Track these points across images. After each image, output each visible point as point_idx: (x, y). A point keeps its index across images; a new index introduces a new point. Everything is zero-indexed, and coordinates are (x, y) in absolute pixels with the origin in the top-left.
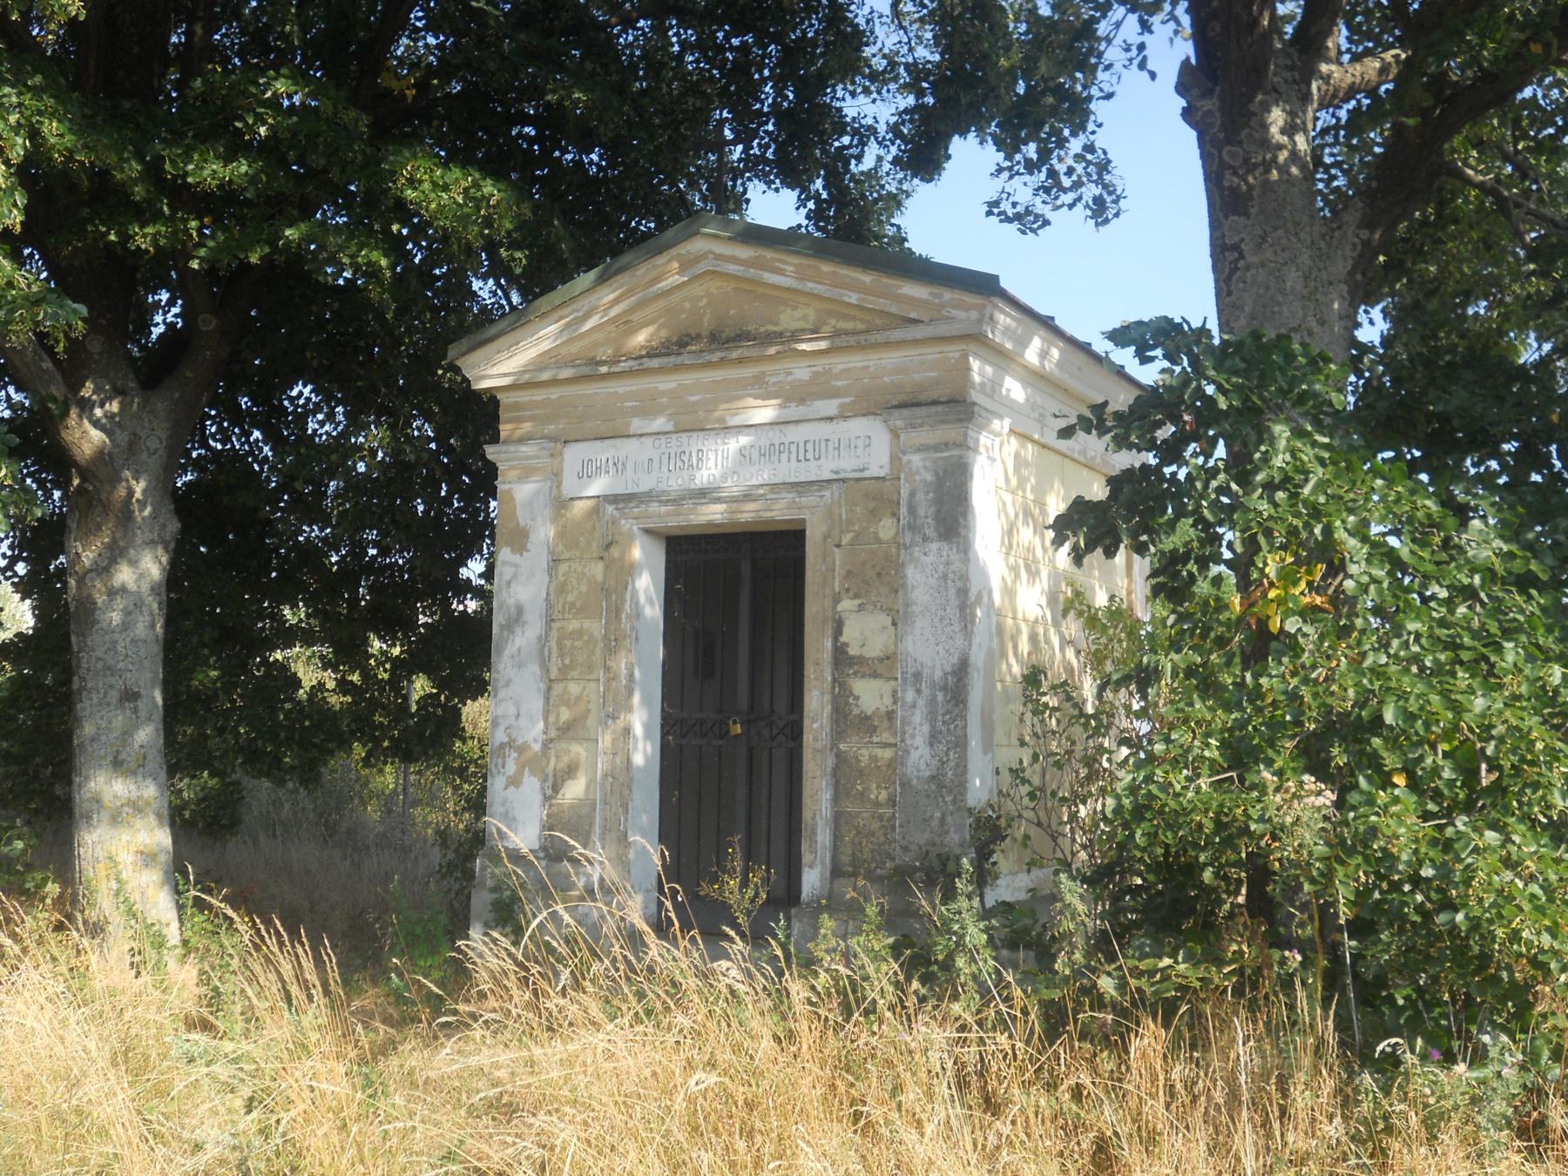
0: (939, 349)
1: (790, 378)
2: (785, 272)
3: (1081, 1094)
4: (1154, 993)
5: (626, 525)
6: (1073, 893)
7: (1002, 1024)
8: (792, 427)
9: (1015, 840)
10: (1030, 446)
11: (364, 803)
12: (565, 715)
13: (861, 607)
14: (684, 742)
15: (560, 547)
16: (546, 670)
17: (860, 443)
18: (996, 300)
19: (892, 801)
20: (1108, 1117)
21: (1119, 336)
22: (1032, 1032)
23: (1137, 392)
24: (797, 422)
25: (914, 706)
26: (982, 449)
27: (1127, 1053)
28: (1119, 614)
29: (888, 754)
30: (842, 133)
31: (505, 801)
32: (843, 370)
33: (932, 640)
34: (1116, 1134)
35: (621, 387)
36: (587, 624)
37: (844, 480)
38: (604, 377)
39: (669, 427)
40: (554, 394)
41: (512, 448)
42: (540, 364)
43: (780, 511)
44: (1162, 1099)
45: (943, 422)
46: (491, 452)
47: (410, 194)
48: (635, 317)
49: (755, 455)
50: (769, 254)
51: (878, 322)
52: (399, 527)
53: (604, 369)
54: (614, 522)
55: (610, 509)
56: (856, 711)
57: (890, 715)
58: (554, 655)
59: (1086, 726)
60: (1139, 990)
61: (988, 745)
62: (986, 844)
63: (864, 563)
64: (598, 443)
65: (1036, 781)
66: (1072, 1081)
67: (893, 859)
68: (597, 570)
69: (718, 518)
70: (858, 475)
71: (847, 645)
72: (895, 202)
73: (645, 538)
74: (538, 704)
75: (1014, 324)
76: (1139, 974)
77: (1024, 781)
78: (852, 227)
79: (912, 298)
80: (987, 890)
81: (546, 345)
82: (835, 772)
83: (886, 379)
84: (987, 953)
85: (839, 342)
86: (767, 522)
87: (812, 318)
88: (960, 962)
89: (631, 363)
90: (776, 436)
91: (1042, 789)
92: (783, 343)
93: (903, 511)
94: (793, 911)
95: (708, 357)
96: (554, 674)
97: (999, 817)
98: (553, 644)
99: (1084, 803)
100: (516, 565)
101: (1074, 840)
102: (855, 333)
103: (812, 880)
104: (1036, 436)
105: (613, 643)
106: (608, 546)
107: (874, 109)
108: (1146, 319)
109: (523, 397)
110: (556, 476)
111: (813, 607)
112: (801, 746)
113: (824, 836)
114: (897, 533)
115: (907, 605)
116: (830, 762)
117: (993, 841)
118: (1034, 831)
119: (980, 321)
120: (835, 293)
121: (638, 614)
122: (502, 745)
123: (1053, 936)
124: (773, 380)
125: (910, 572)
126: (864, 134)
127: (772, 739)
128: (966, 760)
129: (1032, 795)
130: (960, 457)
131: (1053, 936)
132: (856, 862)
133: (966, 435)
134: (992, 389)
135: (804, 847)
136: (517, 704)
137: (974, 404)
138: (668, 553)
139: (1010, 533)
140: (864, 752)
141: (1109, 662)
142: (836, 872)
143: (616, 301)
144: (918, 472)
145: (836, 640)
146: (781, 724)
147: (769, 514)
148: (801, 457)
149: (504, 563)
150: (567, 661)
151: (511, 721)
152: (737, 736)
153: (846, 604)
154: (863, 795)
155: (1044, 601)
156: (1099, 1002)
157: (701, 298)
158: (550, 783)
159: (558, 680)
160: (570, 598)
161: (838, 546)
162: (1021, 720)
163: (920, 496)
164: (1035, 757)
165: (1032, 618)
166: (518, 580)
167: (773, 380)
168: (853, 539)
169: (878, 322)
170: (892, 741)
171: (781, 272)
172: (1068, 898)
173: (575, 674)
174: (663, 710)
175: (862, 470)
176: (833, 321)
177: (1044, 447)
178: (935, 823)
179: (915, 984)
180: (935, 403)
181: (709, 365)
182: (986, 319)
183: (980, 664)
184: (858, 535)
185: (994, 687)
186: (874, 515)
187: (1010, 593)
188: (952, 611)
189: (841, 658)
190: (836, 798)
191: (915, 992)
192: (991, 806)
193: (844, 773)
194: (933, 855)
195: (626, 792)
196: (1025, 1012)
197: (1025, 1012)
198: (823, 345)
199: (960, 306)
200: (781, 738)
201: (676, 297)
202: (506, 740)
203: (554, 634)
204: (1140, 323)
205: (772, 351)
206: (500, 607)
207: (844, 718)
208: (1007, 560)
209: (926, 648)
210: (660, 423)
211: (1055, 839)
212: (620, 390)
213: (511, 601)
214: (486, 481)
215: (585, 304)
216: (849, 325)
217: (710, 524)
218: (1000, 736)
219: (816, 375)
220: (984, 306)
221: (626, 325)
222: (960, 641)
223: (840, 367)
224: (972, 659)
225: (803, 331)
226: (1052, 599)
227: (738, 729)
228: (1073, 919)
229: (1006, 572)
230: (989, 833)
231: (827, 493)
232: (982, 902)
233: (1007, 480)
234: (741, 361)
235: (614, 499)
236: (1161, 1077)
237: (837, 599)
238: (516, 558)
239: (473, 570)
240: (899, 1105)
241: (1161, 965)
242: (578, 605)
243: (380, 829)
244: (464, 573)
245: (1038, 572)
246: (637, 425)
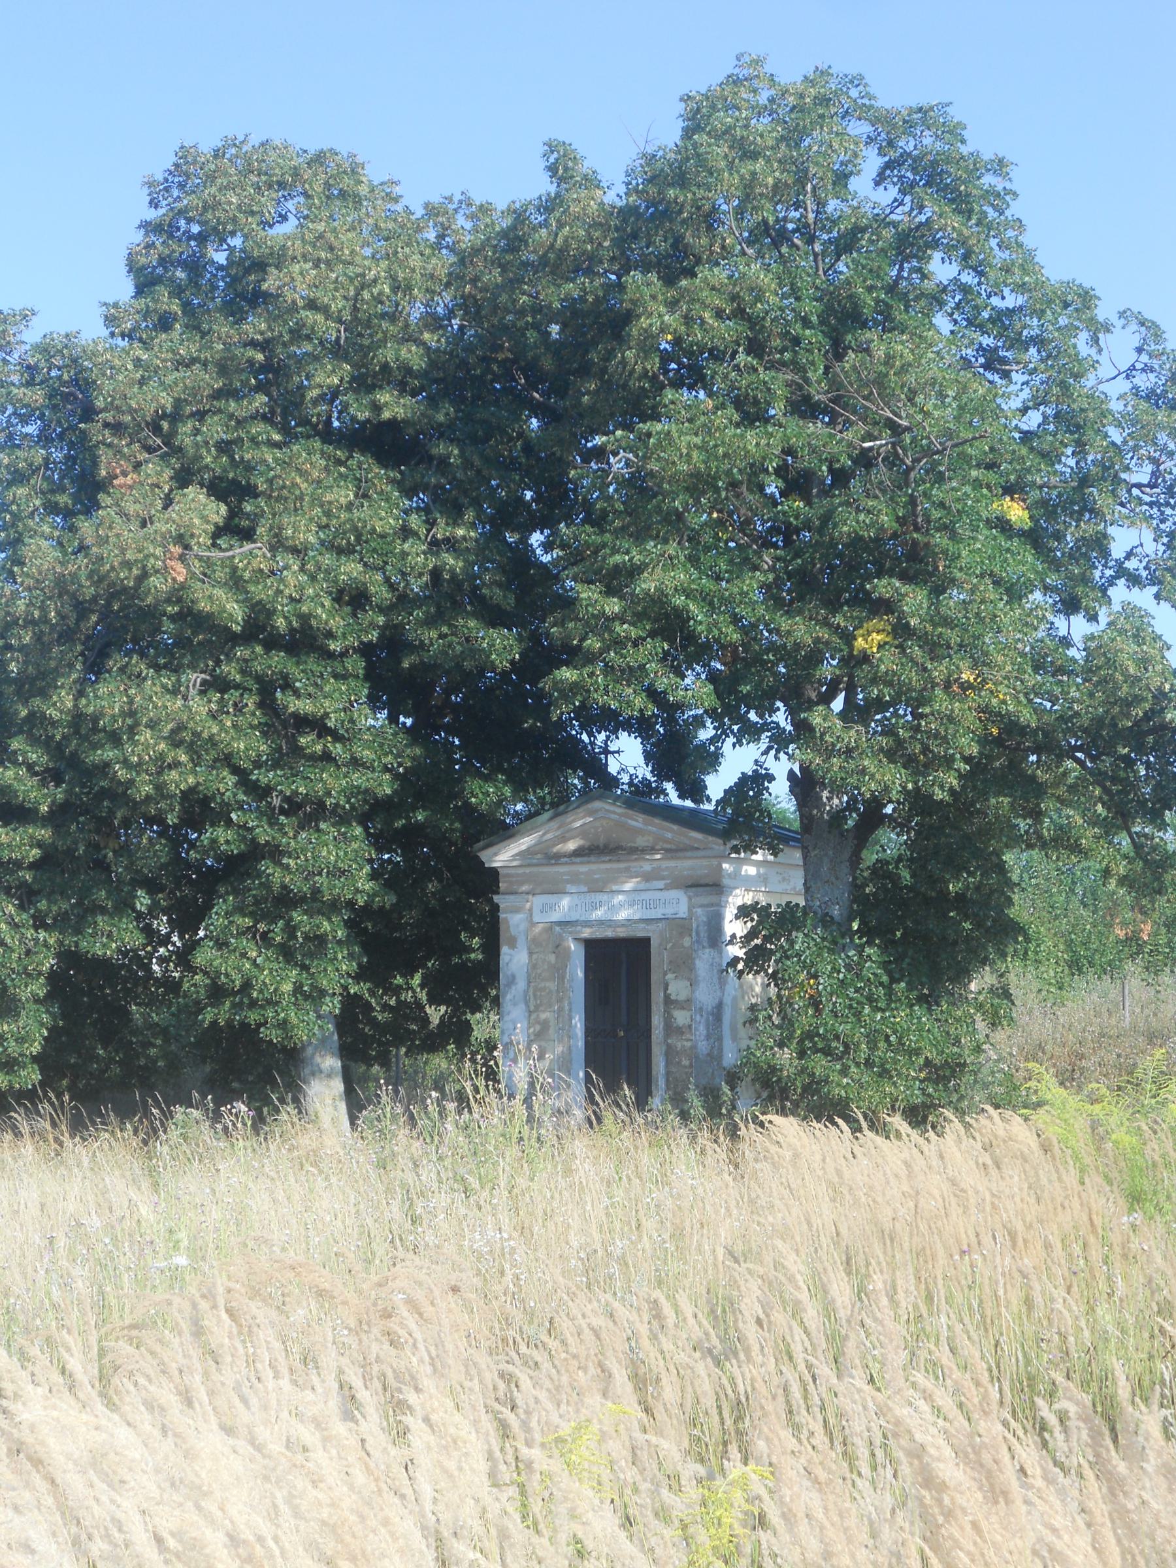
29: (688, 1044)
55: (558, 929)
57: (690, 1026)
61: (735, 1038)
68: (552, 958)
82: (667, 1054)
90: (637, 897)
111: (655, 977)
116: (664, 1048)
125: (697, 962)
140: (680, 1044)
153: (670, 976)
154: (679, 1063)
186: (681, 935)
189: (668, 1001)
190: (667, 1065)
193: (670, 1053)
207: (670, 1028)
209: (705, 996)
222: (719, 993)
237: (665, 974)
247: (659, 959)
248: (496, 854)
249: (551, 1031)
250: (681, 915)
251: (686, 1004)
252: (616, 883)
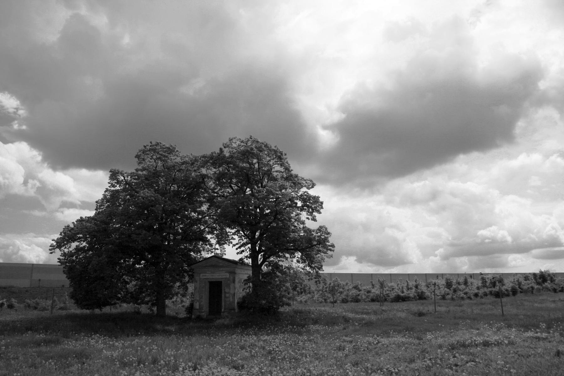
43: (220, 280)
142: (225, 309)
207: (225, 297)
209: (232, 292)
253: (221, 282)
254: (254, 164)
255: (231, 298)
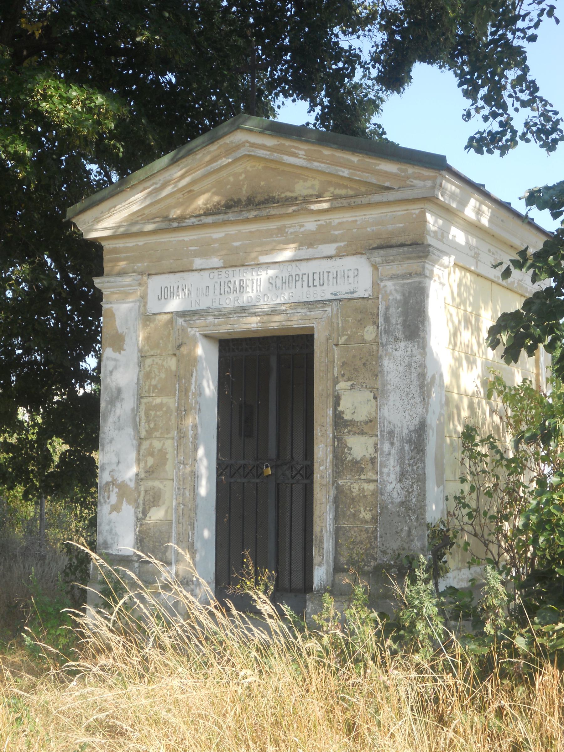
0: (405, 208)
1: (302, 229)
2: (298, 155)
3: (502, 713)
4: (552, 647)
5: (192, 331)
6: (494, 579)
7: (448, 668)
8: (304, 264)
9: (459, 546)
10: (468, 275)
11: (13, 526)
12: (150, 461)
13: (352, 387)
14: (232, 480)
15: (147, 348)
16: (136, 427)
17: (351, 274)
18: (444, 173)
19: (374, 519)
20: (521, 729)
21: (533, 198)
22: (468, 674)
23: (545, 239)
24: (307, 260)
25: (389, 454)
26: (436, 278)
27: (534, 685)
28: (530, 392)
29: (371, 487)
30: (338, 60)
31: (110, 522)
32: (340, 223)
33: (401, 409)
34: (526, 740)
35: (187, 237)
36: (165, 400)
37: (340, 300)
38: (175, 230)
39: (220, 264)
40: (141, 241)
41: (112, 279)
42: (134, 219)
43: (297, 322)
44: (557, 716)
45: (409, 258)
46: (98, 282)
47: (44, 105)
48: (196, 188)
49: (279, 282)
50: (287, 143)
51: (363, 189)
52: (35, 333)
53: (175, 224)
54: (184, 330)
55: (180, 321)
56: (350, 458)
57: (373, 461)
58: (143, 421)
59: (508, 466)
60: (542, 645)
61: (440, 481)
62: (439, 549)
63: (354, 357)
64: (171, 276)
65: (473, 505)
66: (495, 705)
67: (375, 559)
68: (172, 363)
69: (254, 326)
70: (350, 296)
71: (343, 412)
72: (374, 106)
73: (205, 341)
74: (133, 455)
75: (458, 191)
76: (540, 634)
77: (465, 506)
78: (346, 124)
79: (386, 172)
80: (440, 581)
81: (135, 208)
82: (336, 501)
83: (369, 229)
84: (438, 620)
85: (336, 204)
86: (287, 329)
87: (317, 187)
88: (420, 626)
89: (193, 220)
90: (293, 269)
91: (477, 510)
92: (297, 205)
93: (381, 320)
94: (308, 596)
95: (245, 215)
96: (143, 434)
97: (448, 530)
98: (142, 414)
99: (507, 520)
100: (115, 360)
101: (500, 546)
102: (347, 197)
103: (320, 574)
104: (473, 268)
105: (183, 411)
106: (179, 346)
107: (365, 43)
108: (550, 184)
109: (120, 244)
110: (144, 298)
111: (319, 387)
112: (312, 482)
113: (328, 545)
114: (377, 336)
115: (384, 385)
116: (332, 493)
117: (445, 546)
118: (473, 541)
119: (433, 187)
120: (332, 169)
121: (200, 393)
122: (108, 484)
123: (483, 609)
124: (292, 230)
125: (386, 362)
126: (352, 59)
127: (293, 478)
128: (425, 491)
129: (470, 515)
130: (420, 283)
131: (483, 609)
132: (351, 562)
133: (424, 268)
134: (442, 234)
135: (315, 551)
136: (118, 455)
137: (430, 245)
138: (220, 351)
139: (455, 335)
140: (356, 486)
141: (524, 423)
142: (338, 569)
143: (182, 177)
144: (391, 293)
145: (335, 409)
146: (298, 467)
147: (289, 323)
148: (311, 284)
149: (108, 359)
150: (152, 426)
151: (114, 467)
152: (268, 476)
153: (342, 385)
154: (354, 516)
155: (478, 383)
156: (515, 653)
157: (240, 174)
158: (141, 509)
159: (146, 439)
160: (154, 382)
161: (336, 345)
162: (462, 463)
163: (392, 310)
164: (473, 489)
165: (470, 393)
166: (117, 370)
167: (292, 230)
168: (346, 340)
169: (363, 189)
170: (374, 477)
171: (295, 155)
172: (492, 582)
173: (157, 434)
174: (218, 459)
175: (352, 293)
176: (332, 189)
177: (478, 275)
178: (404, 534)
179: (389, 642)
180: (402, 245)
181: (247, 221)
182: (437, 186)
183: (434, 426)
184: (350, 337)
185: (444, 441)
186: (361, 323)
187: (455, 375)
188: (415, 389)
189: (339, 421)
190: (336, 518)
191: (390, 648)
192: (442, 522)
193: (341, 500)
194: (403, 557)
195: (192, 515)
196: (464, 662)
197: (464, 662)
198: (325, 206)
199: (419, 177)
200: (298, 477)
201: (224, 173)
202: (110, 479)
203: (143, 407)
204: (547, 188)
205: (291, 210)
206: (106, 388)
207: (341, 463)
208: (453, 354)
209: (397, 414)
210: (216, 261)
211: (486, 545)
212: (186, 239)
213: (113, 385)
214: (93, 305)
215: (166, 176)
216: (343, 192)
217: (249, 331)
218: (448, 474)
219: (320, 226)
220: (436, 178)
221: (190, 193)
222: (420, 409)
223: (337, 221)
224: (428, 422)
225: (311, 196)
226: (484, 383)
227: (269, 471)
228: (496, 597)
229: (452, 362)
230: (441, 541)
231: (329, 309)
232: (436, 585)
233: (453, 299)
234: (269, 217)
235: (183, 314)
236: (557, 702)
237: (336, 382)
238: (116, 355)
239: (90, 362)
240: (379, 723)
241: (557, 628)
242: (159, 386)
243: (24, 543)
244: (83, 365)
245: (474, 362)
246: (198, 263)
247: (326, 362)
248: (98, 220)
249: (169, 466)
250: (361, 293)
251: (367, 427)
252: (267, 253)
253: (313, 327)
254: (230, 62)
255: (391, 469)
